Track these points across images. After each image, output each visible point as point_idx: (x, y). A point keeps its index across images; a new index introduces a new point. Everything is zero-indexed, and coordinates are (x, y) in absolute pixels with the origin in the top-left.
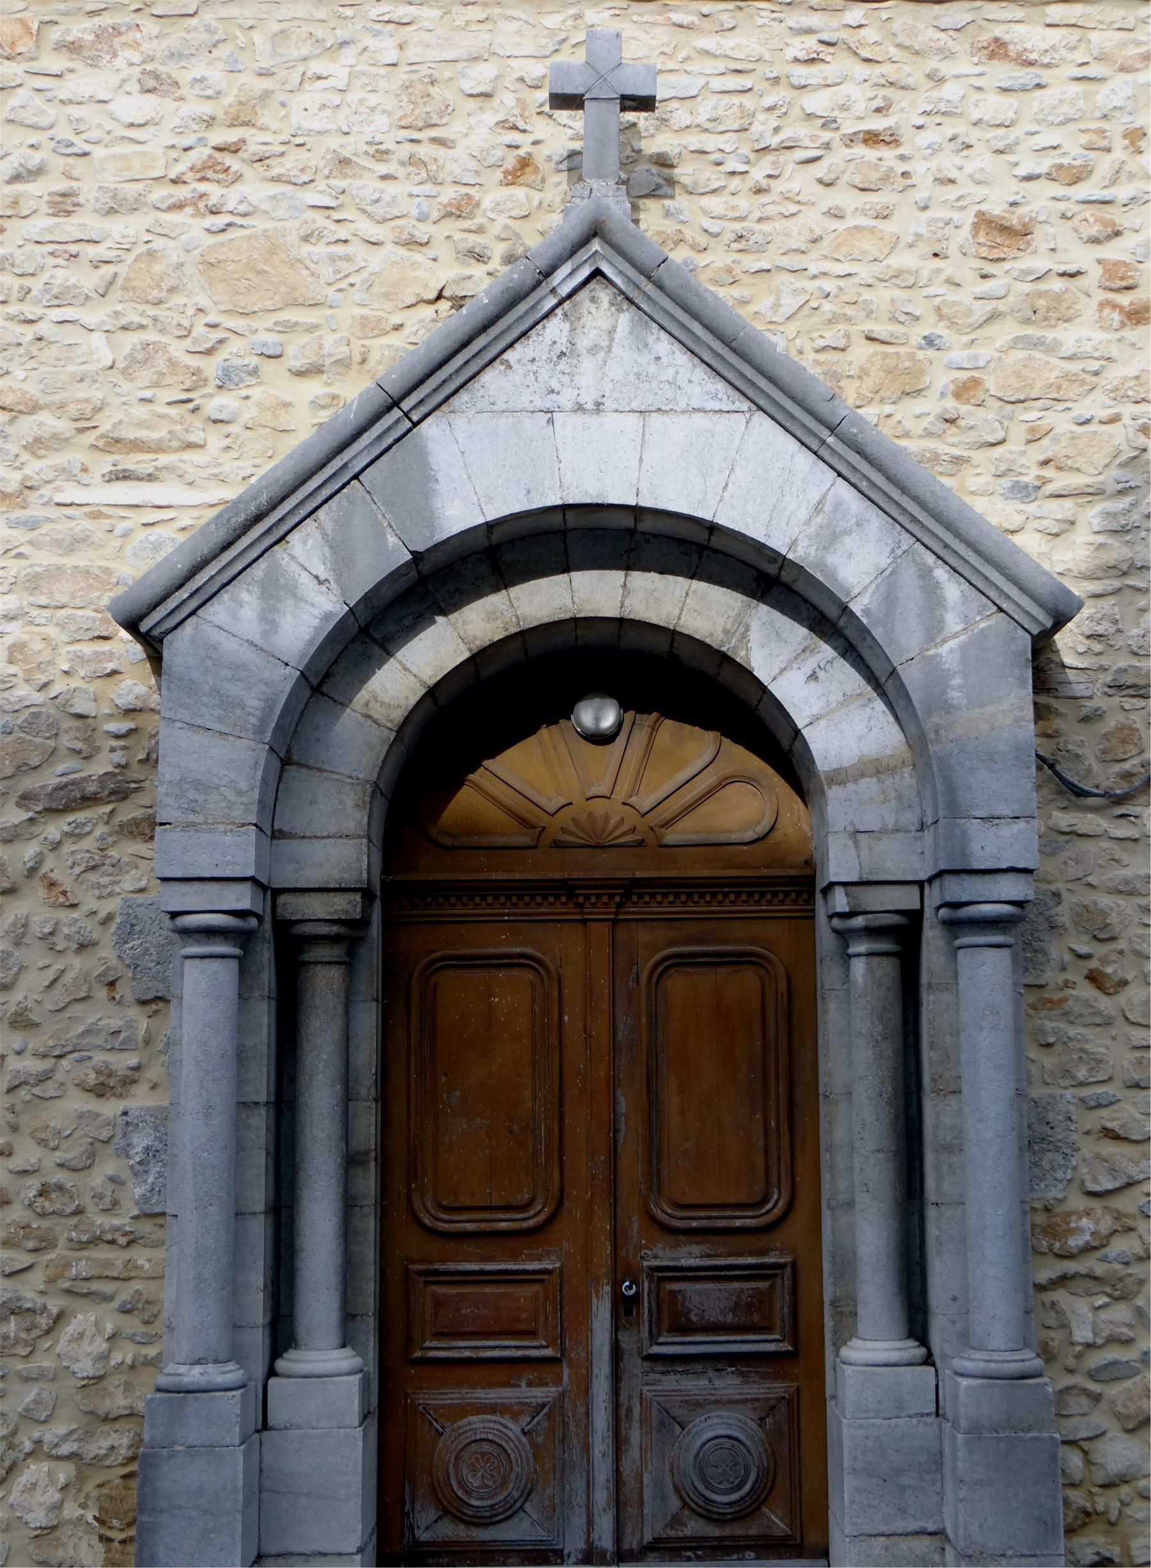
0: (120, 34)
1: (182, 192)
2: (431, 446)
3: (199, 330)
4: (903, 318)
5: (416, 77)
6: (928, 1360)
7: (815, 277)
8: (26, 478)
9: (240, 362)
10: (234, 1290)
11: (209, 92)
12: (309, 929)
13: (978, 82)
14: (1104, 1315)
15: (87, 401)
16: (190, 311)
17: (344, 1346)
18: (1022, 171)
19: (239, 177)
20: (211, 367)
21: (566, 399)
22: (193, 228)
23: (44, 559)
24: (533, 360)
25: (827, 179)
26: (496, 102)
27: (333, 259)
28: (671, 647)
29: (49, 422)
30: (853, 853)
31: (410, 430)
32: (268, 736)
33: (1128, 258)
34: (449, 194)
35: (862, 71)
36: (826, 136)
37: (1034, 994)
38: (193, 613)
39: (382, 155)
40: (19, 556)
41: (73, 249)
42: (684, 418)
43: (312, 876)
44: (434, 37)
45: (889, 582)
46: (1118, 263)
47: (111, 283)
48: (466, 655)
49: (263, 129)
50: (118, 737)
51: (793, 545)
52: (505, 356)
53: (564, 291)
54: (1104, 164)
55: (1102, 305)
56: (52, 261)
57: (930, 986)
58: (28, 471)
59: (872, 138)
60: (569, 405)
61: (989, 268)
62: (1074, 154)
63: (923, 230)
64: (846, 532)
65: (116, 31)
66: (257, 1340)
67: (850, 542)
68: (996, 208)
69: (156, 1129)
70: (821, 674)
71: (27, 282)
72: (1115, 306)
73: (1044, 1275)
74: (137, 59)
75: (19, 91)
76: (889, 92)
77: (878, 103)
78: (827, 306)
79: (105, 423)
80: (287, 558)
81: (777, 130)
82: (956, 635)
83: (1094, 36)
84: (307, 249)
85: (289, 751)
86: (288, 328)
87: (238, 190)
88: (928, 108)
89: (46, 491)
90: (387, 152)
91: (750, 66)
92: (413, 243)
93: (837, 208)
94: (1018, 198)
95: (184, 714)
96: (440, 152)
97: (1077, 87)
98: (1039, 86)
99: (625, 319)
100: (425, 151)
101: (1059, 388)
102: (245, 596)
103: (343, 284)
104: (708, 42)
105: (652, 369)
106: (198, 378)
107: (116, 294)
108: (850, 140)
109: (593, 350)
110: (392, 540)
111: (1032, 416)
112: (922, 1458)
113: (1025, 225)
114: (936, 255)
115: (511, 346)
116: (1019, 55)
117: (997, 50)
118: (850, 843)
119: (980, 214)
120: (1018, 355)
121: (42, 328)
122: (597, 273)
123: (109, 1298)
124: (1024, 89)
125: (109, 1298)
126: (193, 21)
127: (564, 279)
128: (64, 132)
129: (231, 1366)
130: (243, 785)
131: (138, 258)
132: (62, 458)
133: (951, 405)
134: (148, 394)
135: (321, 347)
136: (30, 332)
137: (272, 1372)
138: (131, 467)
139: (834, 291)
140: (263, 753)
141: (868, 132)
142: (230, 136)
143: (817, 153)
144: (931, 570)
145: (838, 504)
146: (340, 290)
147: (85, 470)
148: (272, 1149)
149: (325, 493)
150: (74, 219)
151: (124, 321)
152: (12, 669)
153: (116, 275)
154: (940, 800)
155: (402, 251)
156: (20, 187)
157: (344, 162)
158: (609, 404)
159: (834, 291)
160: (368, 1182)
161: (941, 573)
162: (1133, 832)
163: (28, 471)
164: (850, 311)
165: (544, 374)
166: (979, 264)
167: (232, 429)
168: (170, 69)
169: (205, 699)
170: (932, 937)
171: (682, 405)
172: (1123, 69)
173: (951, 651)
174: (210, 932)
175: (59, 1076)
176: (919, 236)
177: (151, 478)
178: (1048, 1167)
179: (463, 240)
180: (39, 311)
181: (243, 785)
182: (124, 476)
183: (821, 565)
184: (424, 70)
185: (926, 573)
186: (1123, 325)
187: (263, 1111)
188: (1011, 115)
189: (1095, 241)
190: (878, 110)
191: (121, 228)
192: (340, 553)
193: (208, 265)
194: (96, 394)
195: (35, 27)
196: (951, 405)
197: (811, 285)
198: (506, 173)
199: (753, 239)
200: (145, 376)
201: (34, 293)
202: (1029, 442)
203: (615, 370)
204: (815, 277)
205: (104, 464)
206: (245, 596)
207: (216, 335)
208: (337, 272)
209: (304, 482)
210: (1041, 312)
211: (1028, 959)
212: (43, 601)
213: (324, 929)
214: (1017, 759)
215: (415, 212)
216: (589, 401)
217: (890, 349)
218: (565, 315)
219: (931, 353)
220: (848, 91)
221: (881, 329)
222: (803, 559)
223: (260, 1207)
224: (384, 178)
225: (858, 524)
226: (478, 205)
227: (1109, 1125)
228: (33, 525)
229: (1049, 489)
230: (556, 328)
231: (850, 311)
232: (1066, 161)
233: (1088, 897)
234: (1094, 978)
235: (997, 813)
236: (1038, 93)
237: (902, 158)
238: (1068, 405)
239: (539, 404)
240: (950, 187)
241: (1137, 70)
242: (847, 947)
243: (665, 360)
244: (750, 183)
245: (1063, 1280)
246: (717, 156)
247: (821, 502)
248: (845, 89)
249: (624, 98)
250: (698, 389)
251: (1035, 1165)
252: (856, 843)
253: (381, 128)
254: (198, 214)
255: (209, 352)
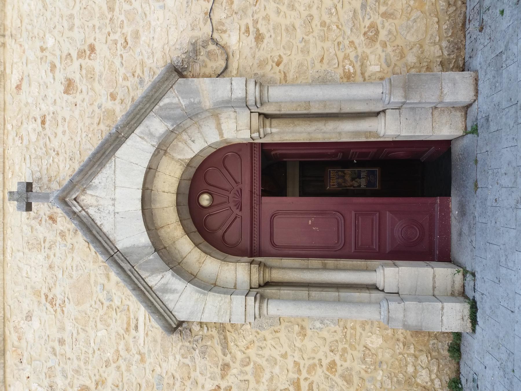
0: (16, 326)
1: (59, 310)
2: (125, 246)
3: (97, 306)
4: (93, 115)
5: (27, 247)
6: (384, 111)
7: (82, 139)
8: (137, 353)
9: (105, 295)
10: (360, 303)
11: (31, 303)
12: (261, 279)
13: (28, 93)
14: (373, 63)
15: (116, 337)
16: (91, 308)
17: (376, 271)
18: (52, 81)
19: (55, 295)
20: (106, 303)
21: (111, 208)
22: (69, 307)
23: (159, 348)
24: (100, 218)
25: (55, 135)
26: (33, 225)
27: (77, 270)
28: (187, 180)
29: (121, 347)
30: (242, 131)
31: (120, 252)
32: (206, 292)
33: (77, 51)
34: (59, 239)
35: (25, 125)
36: (42, 135)
37: (285, 81)
38: (171, 312)
39: (48, 257)
40: (158, 355)
41: (74, 340)
42: (117, 175)
43: (246, 278)
44: (14, 242)
45: (164, 118)
46: (78, 55)
47: (84, 330)
48: (186, 236)
49: (41, 288)
50: (208, 329)
51: (153, 146)
52: (99, 225)
53: (80, 209)
54: (50, 58)
55: (90, 59)
56: (78, 346)
57: (280, 111)
58: (135, 353)
59: (43, 122)
60: (113, 207)
61: (79, 90)
62: (47, 67)
63: (69, 109)
64: (149, 131)
65: (15, 327)
66: (375, 295)
67: (152, 130)
68: (62, 88)
69: (315, 320)
70: (193, 139)
71: (83, 352)
72: (90, 56)
73: (361, 79)
74: (22, 322)
75: (31, 353)
76: (30, 118)
77: (33, 120)
78: (90, 135)
79: (122, 332)
80: (156, 286)
81: (41, 149)
82: (179, 100)
83: (15, 60)
84: (74, 277)
85: (212, 284)
86: (96, 282)
87: (59, 296)
88: (35, 106)
89: (141, 348)
90: (47, 255)
91: (23, 156)
92: (72, 249)
93: (62, 132)
94: (60, 82)
95: (200, 314)
96: (47, 240)
97: (29, 66)
98: (29, 76)
99: (89, 192)
100: (47, 245)
101: (113, 71)
102: (166, 298)
103: (84, 267)
104: (17, 167)
105: (103, 184)
106: (109, 307)
107: (87, 329)
108: (44, 128)
109: (97, 201)
110: (151, 257)
111: (121, 79)
112: (411, 113)
113: (67, 80)
114: (76, 105)
115: (96, 224)
116: (20, 81)
117: (18, 87)
118: (240, 132)
119: (64, 93)
120: (103, 82)
121: (96, 349)
122: (75, 199)
123: (361, 334)
124: (30, 80)
125: (361, 334)
126: (12, 306)
127: (77, 209)
128: (43, 342)
129: (381, 304)
130: (220, 299)
131: (77, 323)
132: (132, 345)
133: (118, 101)
134: (114, 321)
135: (101, 274)
136: (97, 352)
137: (383, 291)
138: (134, 325)
139: (86, 133)
140: (211, 293)
141: (42, 124)
142: (43, 297)
143: (47, 137)
144: (160, 107)
145: (142, 133)
146: (85, 268)
147: (135, 338)
148: (321, 289)
149: (137, 276)
150: (66, 339)
151: (94, 327)
152: (189, 357)
153: (81, 329)
154: (226, 105)
155: (75, 251)
156: (58, 353)
157: (50, 267)
158: (113, 197)
159: (86, 133)
160: (331, 262)
161: (161, 104)
162: (238, 52)
163: (135, 353)
164: (91, 129)
165: (104, 214)
166: (78, 93)
167: (124, 298)
168: (25, 312)
169: (195, 309)
170: (266, 110)
171: (113, 176)
172: (24, 52)
173: (184, 101)
174: (260, 308)
175: (300, 346)
176: (71, 110)
177: (137, 320)
178: (331, 78)
179: (72, 235)
180: (91, 349)
181: (220, 299)
182: (136, 327)
183: (159, 138)
184: (25, 245)
185: (161, 108)
186: (95, 53)
187: (311, 292)
188: (36, 84)
189: (72, 60)
190: (35, 121)
191: (69, 327)
192: (154, 271)
193: (78, 303)
194: (114, 334)
195: (14, 349)
196: (118, 101)
197: (84, 140)
198: (54, 223)
199: (71, 156)
200: (109, 321)
201: (86, 350)
202: (128, 80)
203: (103, 195)
204: (82, 139)
205: (133, 332)
206: (166, 298)
207: (99, 303)
208: (80, 269)
209: (134, 282)
210: (92, 76)
211: (272, 83)
212: (170, 349)
213: (262, 275)
214: (214, 83)
215: (64, 248)
216: (111, 202)
217: (102, 118)
218: (87, 209)
219: (103, 107)
220: (32, 128)
221: (96, 120)
222: (157, 143)
223: (337, 294)
224: (54, 255)
225: (147, 127)
226: (62, 231)
227: (319, 60)
228: (149, 351)
229: (141, 75)
230: (91, 211)
231: (91, 129)
232: (49, 69)
233: (256, 65)
234: (278, 64)
235: (230, 89)
236: (31, 76)
237: (49, 114)
238: (117, 69)
239: (112, 216)
240: (57, 101)
241: (24, 49)
242: (268, 133)
243: (100, 181)
244: (56, 156)
245: (363, 74)
246: (48, 165)
247: (141, 137)
248: (29, 129)
249: (27, 191)
250: (108, 171)
251: (330, 81)
252: (239, 130)
253: (41, 257)
254: (65, 306)
255: (102, 304)
